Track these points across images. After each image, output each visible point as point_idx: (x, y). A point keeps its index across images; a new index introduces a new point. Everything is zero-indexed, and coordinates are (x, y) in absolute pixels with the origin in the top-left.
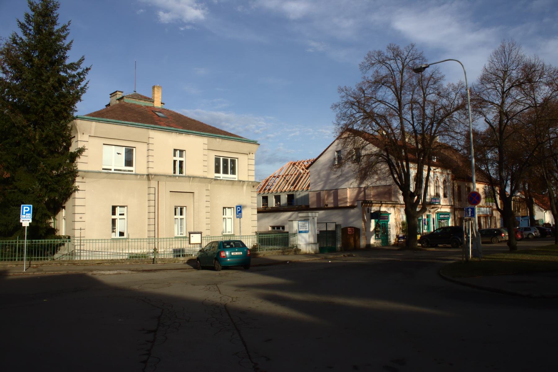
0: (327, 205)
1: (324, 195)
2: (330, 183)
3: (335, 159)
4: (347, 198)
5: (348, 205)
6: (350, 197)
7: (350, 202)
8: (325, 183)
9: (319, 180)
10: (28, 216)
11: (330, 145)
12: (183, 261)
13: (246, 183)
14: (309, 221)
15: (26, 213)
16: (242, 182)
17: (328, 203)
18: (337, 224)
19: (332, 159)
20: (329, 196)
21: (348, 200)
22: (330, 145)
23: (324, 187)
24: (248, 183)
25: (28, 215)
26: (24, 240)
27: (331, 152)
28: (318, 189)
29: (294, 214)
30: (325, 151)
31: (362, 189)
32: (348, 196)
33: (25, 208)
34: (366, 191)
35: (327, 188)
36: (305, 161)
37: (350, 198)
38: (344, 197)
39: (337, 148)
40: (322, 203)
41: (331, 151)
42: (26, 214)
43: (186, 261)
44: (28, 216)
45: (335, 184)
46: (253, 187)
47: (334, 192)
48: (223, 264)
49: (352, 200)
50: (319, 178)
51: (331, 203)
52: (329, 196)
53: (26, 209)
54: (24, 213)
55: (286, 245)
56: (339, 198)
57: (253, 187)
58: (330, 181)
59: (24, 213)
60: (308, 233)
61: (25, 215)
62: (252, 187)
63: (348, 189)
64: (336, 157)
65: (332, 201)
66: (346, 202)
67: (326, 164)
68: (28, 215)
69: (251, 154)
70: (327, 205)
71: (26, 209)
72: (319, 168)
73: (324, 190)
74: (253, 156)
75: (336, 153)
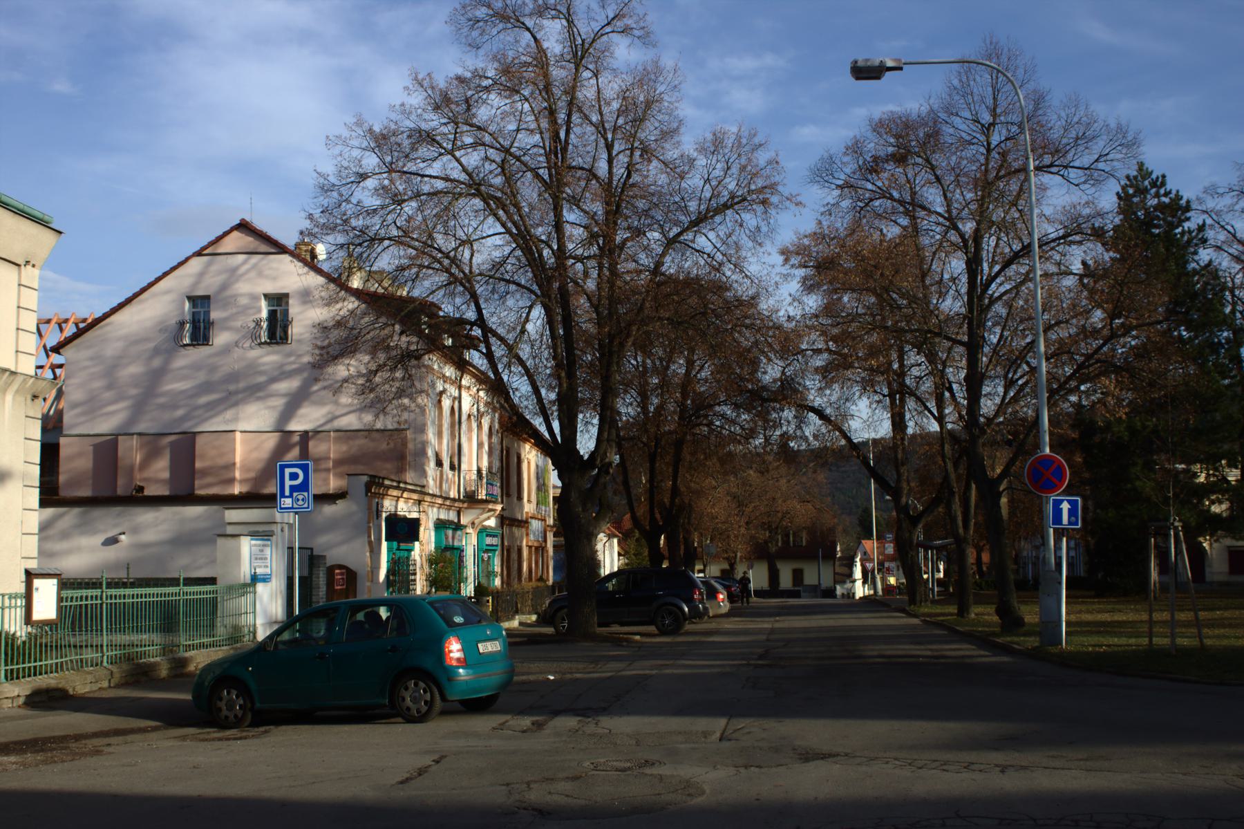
0: (141, 489)
1: (132, 452)
2: (163, 407)
3: (182, 324)
4: (234, 464)
5: (237, 490)
6: (242, 461)
7: (242, 481)
8: (139, 408)
9: (108, 395)
10: (300, 502)
11: (166, 274)
12: (13, 698)
13: (19, 379)
14: (274, 538)
15: (293, 489)
16: (8, 373)
17: (145, 480)
18: (314, 553)
19: (173, 321)
20: (152, 454)
21: (237, 475)
22: (166, 274)
23: (132, 420)
24: (24, 380)
25: (300, 497)
26: (1073, 618)
27: (168, 298)
28: (105, 426)
29: (61, 516)
30: (143, 290)
31: (296, 438)
32: (238, 459)
33: (288, 471)
34: (311, 444)
35: (142, 427)
36: (66, 321)
37: (245, 468)
38: (221, 462)
39: (195, 285)
40: (121, 482)
41: (167, 292)
42: (295, 494)
43: (21, 700)
44: (300, 502)
45: (180, 412)
46: (35, 397)
47: (172, 444)
48: (454, 695)
49: (252, 475)
50: (109, 387)
51: (162, 481)
52: (152, 454)
53: (294, 476)
54: (287, 493)
55: (168, 632)
56: (198, 465)
57: (35, 397)
58: (162, 400)
59: (287, 493)
60: (270, 584)
61: (291, 496)
62: (29, 397)
63: (238, 435)
64: (188, 317)
65: (166, 475)
66: (231, 481)
67: (146, 340)
68: (300, 497)
69: (29, 267)
70: (141, 489)
71: (294, 476)
72: (111, 350)
73: (133, 434)
74: (31, 275)
75: (187, 305)
